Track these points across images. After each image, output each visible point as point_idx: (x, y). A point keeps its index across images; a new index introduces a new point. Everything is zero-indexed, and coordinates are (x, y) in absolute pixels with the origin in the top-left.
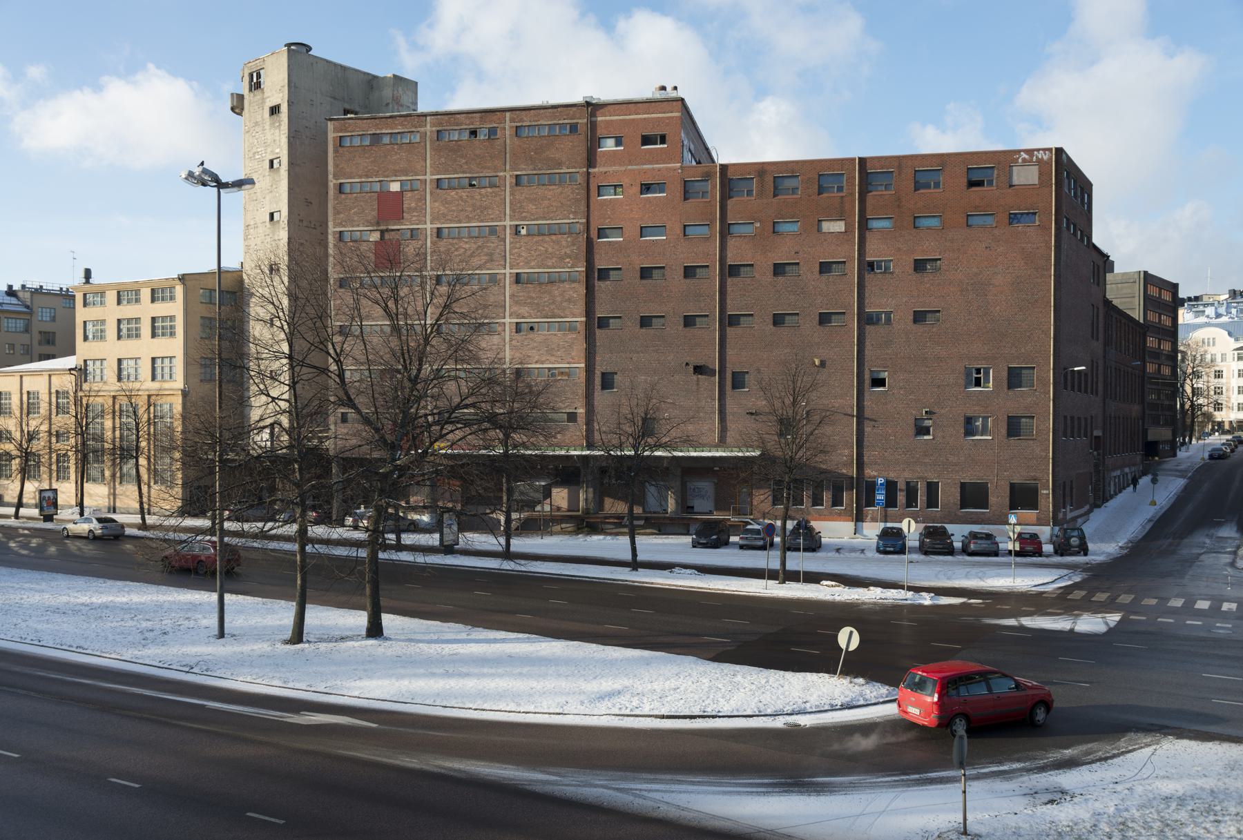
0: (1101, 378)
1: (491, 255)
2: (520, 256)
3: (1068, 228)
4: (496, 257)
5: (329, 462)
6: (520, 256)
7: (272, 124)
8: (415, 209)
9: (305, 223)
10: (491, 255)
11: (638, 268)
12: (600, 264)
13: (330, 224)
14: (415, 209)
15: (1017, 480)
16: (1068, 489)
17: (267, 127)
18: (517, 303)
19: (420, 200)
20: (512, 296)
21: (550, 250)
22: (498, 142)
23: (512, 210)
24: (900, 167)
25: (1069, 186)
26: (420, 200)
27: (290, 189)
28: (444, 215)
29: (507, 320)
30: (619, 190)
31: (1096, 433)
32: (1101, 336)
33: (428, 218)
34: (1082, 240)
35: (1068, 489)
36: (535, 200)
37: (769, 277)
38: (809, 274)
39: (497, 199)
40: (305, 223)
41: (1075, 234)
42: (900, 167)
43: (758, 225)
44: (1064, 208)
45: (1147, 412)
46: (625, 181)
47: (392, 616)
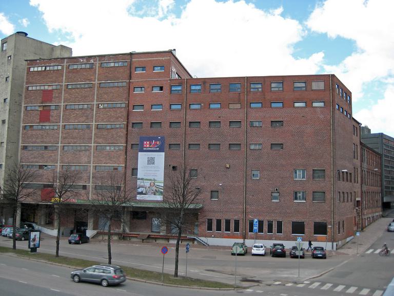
0: (359, 176)
1: (87, 116)
2: (99, 117)
3: (339, 109)
4: (89, 117)
5: (185, 213)
6: (99, 117)
7: (8, 64)
8: (57, 97)
9: (17, 103)
10: (87, 116)
11: (150, 123)
12: (133, 120)
13: (23, 103)
14: (57, 97)
15: (317, 220)
16: (341, 225)
17: (6, 64)
18: (97, 137)
19: (59, 93)
20: (95, 134)
21: (113, 114)
22: (93, 69)
23: (97, 97)
24: (264, 81)
25: (333, 93)
26: (59, 93)
27: (12, 89)
28: (69, 99)
29: (93, 145)
30: (143, 89)
31: (357, 199)
32: (359, 157)
33: (63, 101)
34: (347, 115)
35: (341, 225)
36: (107, 93)
37: (207, 128)
38: (204, 127)
39: (92, 93)
40: (17, 103)
41: (343, 112)
42: (264, 81)
43: (202, 105)
44: (336, 100)
45: (384, 190)
46: (146, 86)
47: (24, 249)
